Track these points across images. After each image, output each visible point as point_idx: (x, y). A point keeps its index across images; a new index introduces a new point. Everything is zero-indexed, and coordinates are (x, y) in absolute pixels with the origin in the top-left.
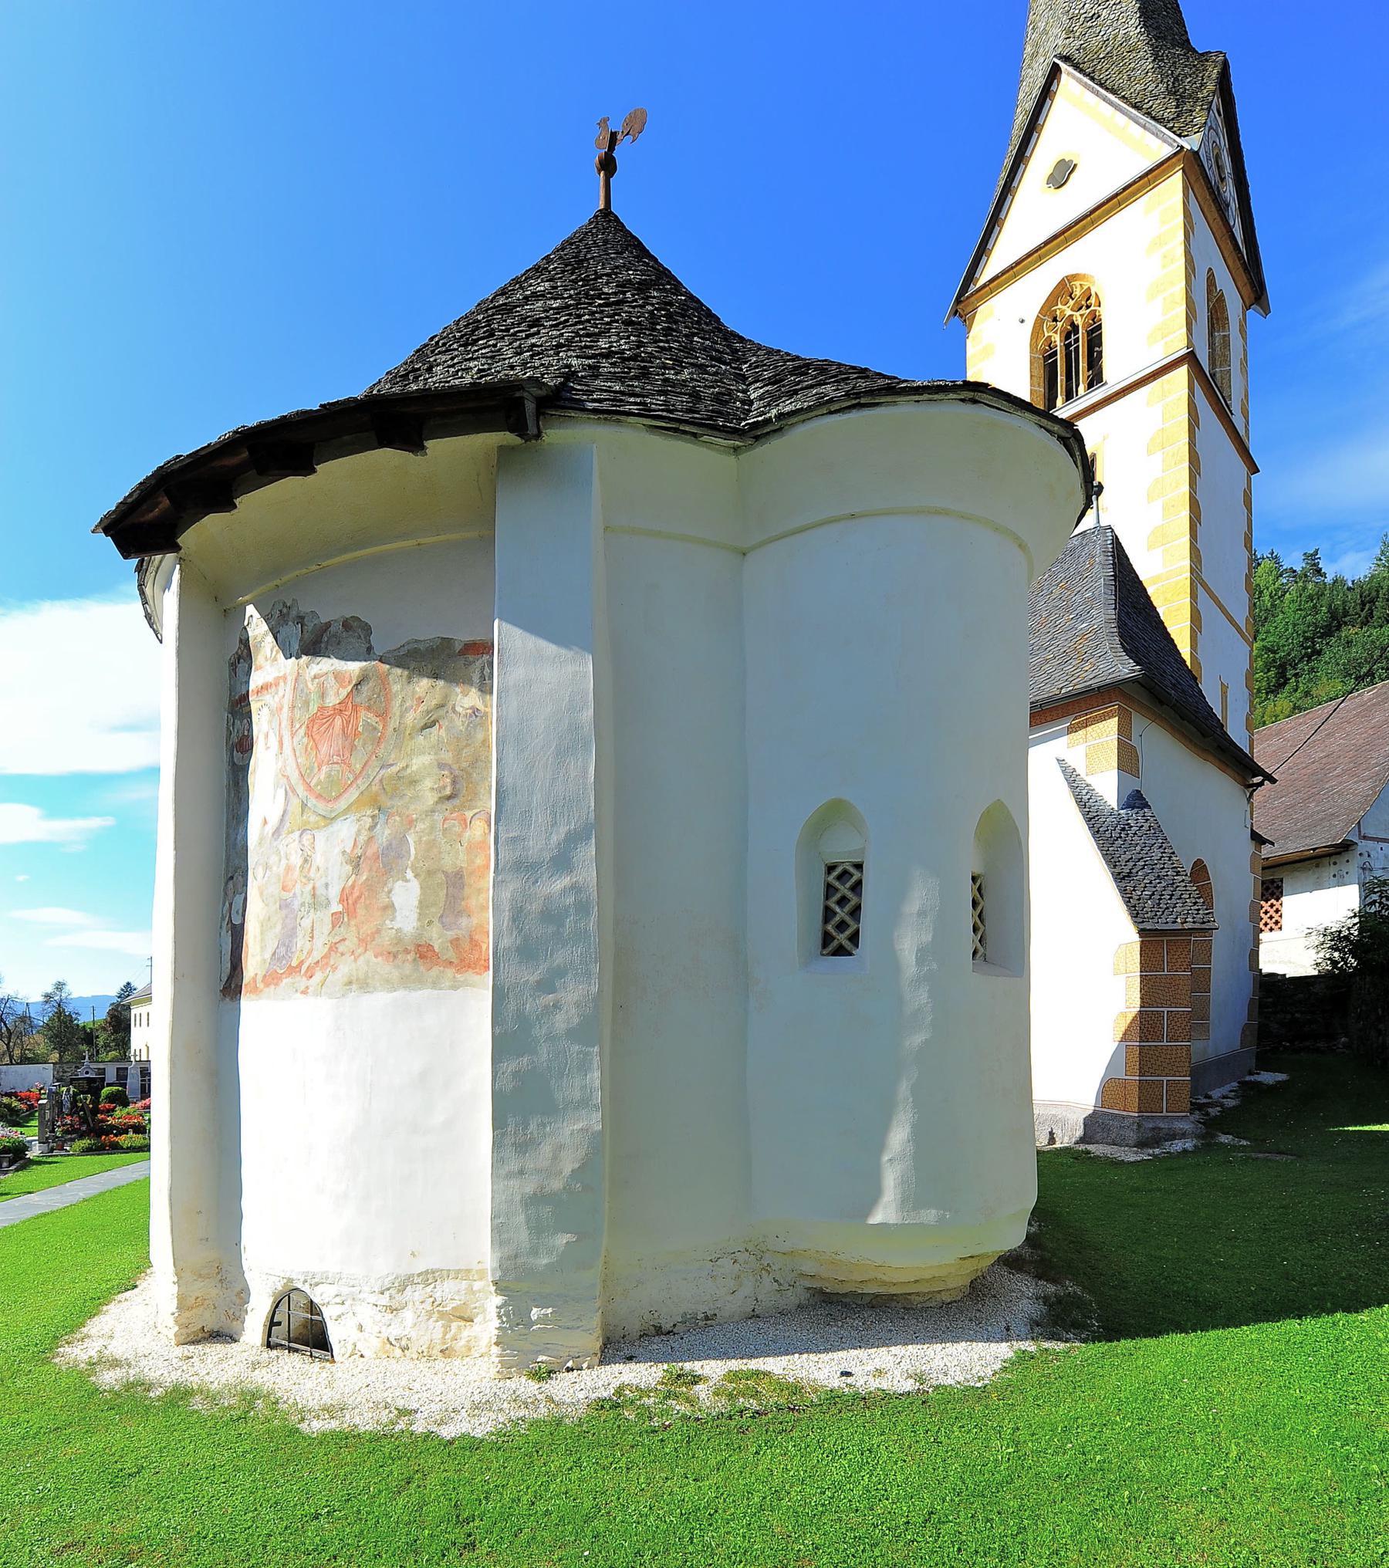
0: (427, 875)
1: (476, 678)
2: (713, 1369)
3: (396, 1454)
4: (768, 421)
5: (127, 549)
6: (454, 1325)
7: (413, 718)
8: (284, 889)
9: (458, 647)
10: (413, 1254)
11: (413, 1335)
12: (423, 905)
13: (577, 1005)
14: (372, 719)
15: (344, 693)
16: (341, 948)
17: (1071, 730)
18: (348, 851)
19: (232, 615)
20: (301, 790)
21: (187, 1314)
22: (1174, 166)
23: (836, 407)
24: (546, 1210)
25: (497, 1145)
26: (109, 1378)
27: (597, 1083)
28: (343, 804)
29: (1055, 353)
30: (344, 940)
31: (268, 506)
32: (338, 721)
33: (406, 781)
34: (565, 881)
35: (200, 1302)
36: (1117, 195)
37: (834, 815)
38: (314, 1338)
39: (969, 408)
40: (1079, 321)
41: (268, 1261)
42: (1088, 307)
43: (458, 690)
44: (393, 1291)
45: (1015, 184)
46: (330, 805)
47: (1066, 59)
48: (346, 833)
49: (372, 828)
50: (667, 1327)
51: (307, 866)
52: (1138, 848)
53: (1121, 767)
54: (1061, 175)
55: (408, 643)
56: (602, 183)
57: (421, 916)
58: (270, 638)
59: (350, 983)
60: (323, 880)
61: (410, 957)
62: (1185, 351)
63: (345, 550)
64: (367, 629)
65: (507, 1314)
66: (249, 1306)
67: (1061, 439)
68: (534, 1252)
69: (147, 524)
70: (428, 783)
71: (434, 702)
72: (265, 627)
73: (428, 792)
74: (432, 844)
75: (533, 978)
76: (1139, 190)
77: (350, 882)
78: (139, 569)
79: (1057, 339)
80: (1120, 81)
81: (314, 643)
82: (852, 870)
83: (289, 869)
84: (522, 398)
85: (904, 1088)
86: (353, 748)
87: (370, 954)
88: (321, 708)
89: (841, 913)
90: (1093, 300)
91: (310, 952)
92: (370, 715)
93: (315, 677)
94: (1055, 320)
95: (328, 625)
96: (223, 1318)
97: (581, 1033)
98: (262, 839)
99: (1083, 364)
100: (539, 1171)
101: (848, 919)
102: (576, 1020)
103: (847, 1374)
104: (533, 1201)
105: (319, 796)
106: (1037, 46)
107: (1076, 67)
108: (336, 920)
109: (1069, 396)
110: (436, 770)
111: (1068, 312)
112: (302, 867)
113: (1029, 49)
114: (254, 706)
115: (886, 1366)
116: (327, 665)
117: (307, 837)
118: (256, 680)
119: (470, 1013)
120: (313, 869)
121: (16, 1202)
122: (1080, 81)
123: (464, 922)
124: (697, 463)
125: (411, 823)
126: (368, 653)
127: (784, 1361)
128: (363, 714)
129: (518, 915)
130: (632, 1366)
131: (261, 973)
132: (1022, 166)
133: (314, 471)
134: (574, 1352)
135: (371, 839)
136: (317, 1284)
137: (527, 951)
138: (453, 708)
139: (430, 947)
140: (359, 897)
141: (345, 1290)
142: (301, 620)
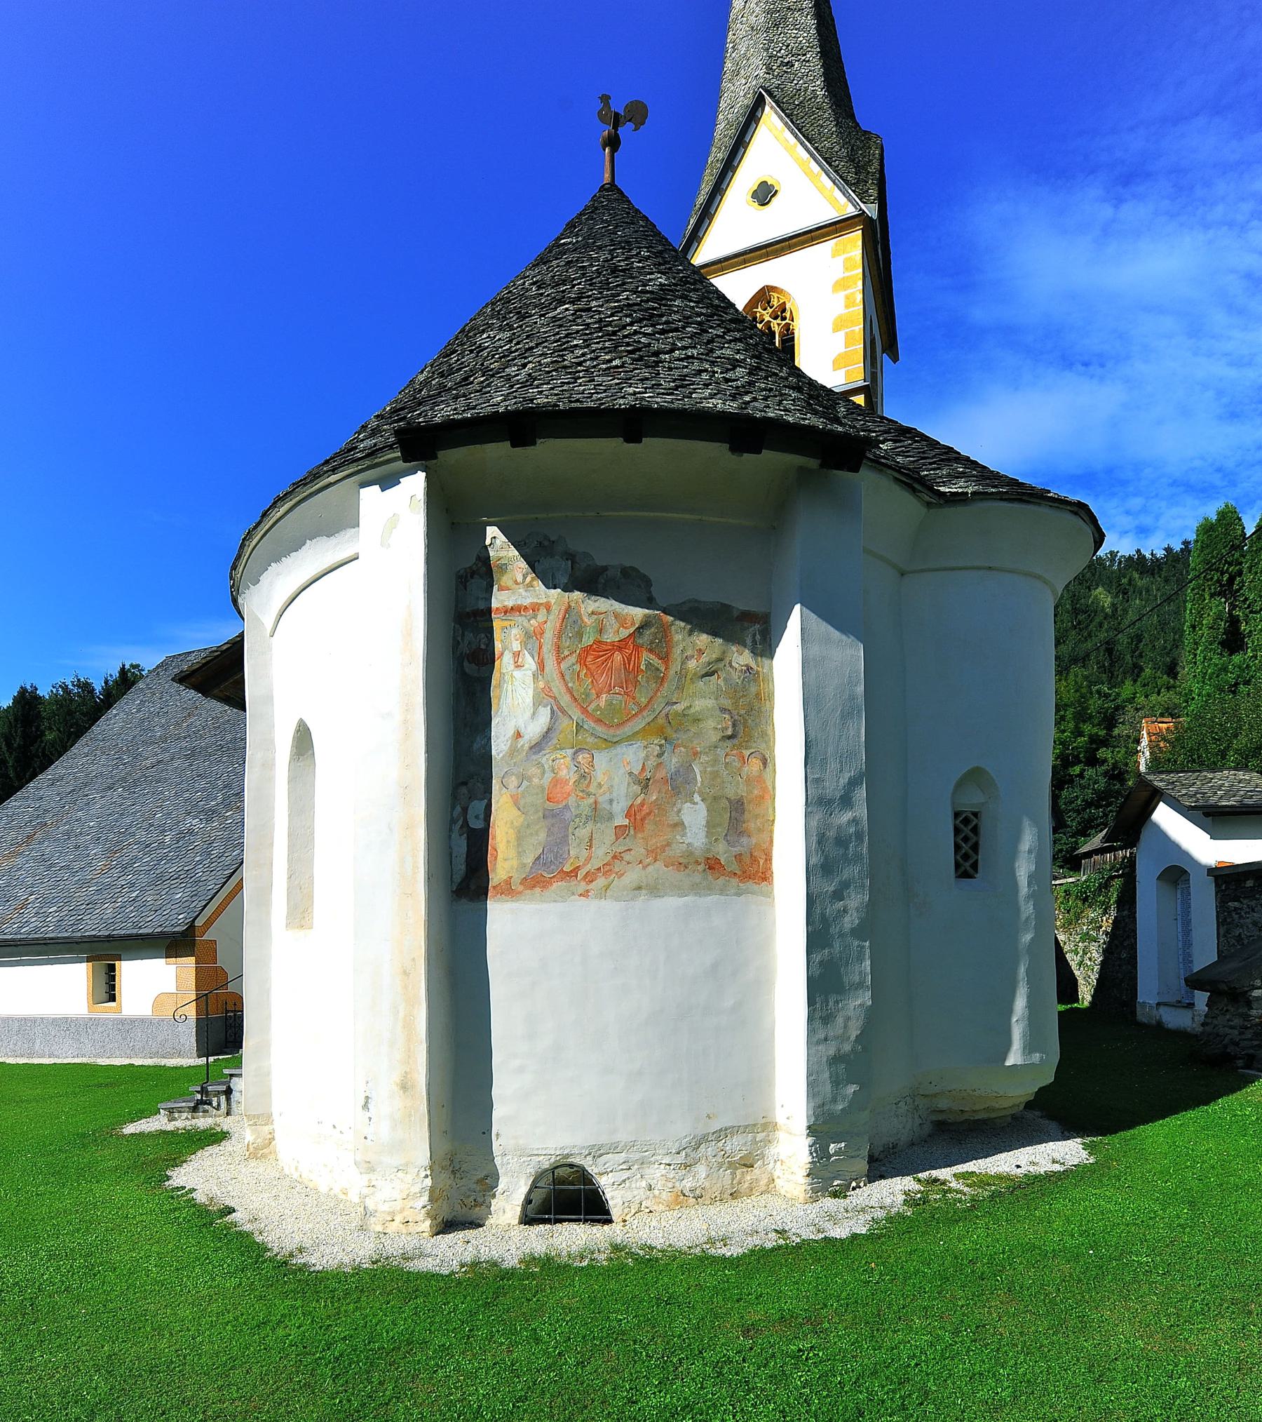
0: (713, 801)
1: (749, 642)
6: (738, 1172)
9: (736, 614)
10: (708, 1116)
11: (707, 1184)
12: (710, 825)
13: (857, 909)
14: (656, 661)
15: (624, 633)
16: (627, 857)
25: (810, 1019)
33: (688, 720)
37: (975, 776)
40: (776, 329)
46: (612, 731)
48: (633, 756)
49: (660, 755)
54: (764, 194)
55: (690, 601)
56: (607, 158)
59: (639, 888)
60: (607, 797)
61: (701, 868)
65: (816, 1151)
70: (711, 723)
71: (714, 656)
73: (712, 728)
74: (715, 775)
75: (832, 889)
77: (639, 801)
87: (659, 864)
91: (589, 859)
92: (652, 656)
93: (593, 613)
95: (605, 569)
96: (458, 1207)
98: (513, 751)
100: (836, 1038)
101: (971, 852)
104: (835, 1060)
107: (777, 102)
108: (620, 831)
110: (718, 712)
111: (767, 318)
113: (728, 65)
120: (594, 784)
123: (744, 840)
125: (695, 754)
126: (648, 602)
128: (646, 656)
136: (601, 1155)
138: (730, 663)
139: (718, 861)
140: (649, 814)
142: (571, 557)
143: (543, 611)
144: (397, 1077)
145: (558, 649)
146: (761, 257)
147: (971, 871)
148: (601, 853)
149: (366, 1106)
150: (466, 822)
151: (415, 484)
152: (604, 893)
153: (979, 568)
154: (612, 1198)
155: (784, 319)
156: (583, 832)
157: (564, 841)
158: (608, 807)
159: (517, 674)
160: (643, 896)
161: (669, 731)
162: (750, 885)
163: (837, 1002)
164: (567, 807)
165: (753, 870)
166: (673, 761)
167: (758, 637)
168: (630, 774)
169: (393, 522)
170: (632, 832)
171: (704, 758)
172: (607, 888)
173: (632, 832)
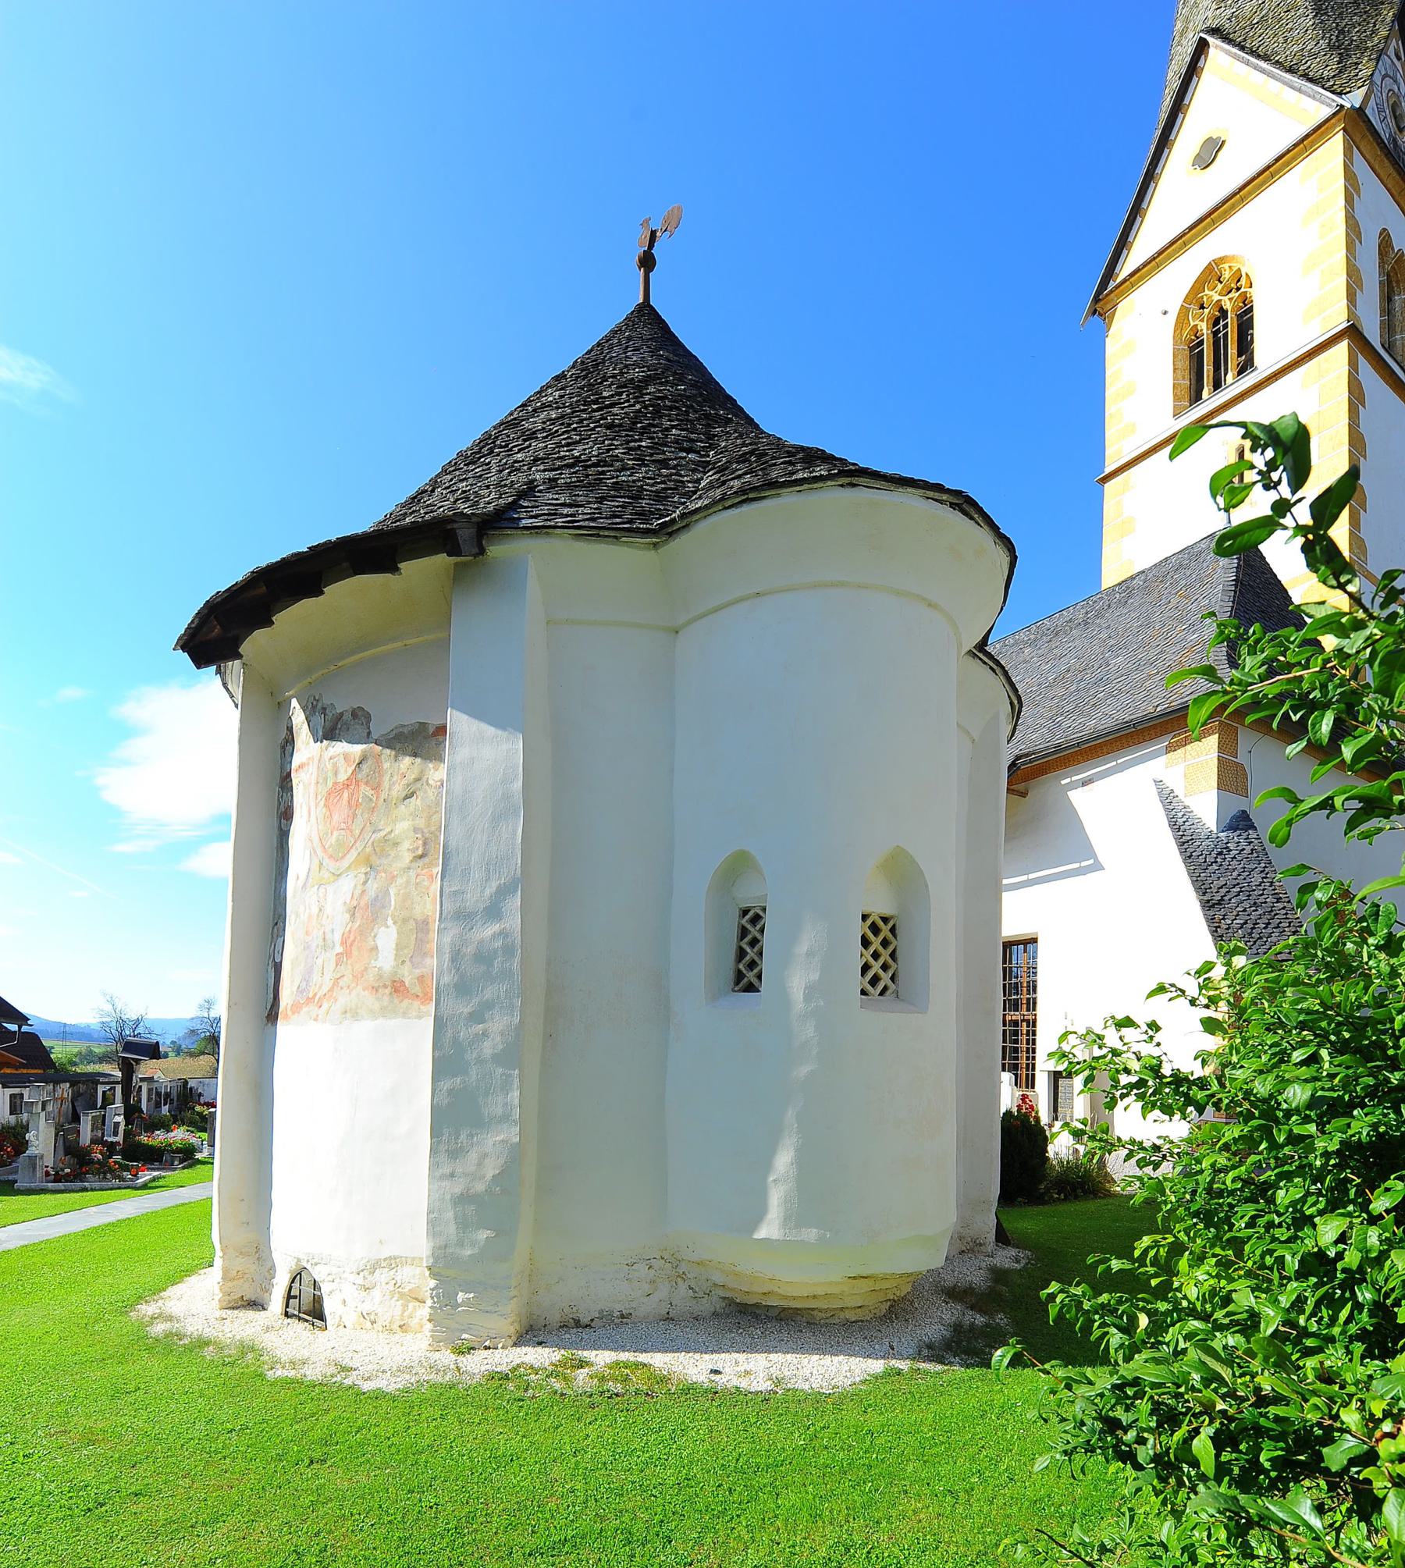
2: (602, 1358)
3: (329, 1396)
4: (673, 521)
5: (200, 661)
6: (411, 1305)
7: (398, 790)
8: (307, 933)
9: (431, 730)
12: (399, 947)
13: (502, 1033)
14: (369, 792)
15: (350, 771)
16: (341, 983)
17: (1170, 749)
19: (282, 706)
20: (320, 854)
21: (230, 1284)
22: (1334, 126)
23: (729, 503)
24: (471, 1209)
25: (433, 1151)
26: (159, 1328)
27: (516, 1101)
28: (346, 863)
29: (1201, 343)
31: (296, 620)
32: (346, 795)
33: (388, 844)
34: (496, 928)
35: (240, 1275)
36: (1269, 167)
37: (739, 866)
38: (316, 1313)
39: (849, 491)
40: (1228, 306)
41: (289, 1244)
42: (1238, 289)
43: (431, 765)
44: (366, 1273)
45: (1158, 170)
47: (1215, 31)
48: (346, 887)
49: (365, 883)
50: (585, 1320)
52: (1235, 874)
53: (1221, 786)
54: (1209, 153)
58: (306, 725)
61: (387, 991)
62: (1345, 325)
63: (353, 653)
64: (368, 717)
66: (275, 1281)
67: (952, 505)
68: (460, 1244)
69: (214, 636)
72: (302, 716)
76: (1294, 159)
78: (218, 672)
79: (1204, 327)
80: (1272, 45)
81: (330, 731)
83: (310, 917)
84: (454, 529)
85: (790, 1115)
86: (355, 816)
87: (360, 988)
88: (335, 783)
89: (751, 953)
90: (1243, 281)
94: (1202, 307)
95: (342, 714)
97: (510, 1056)
99: (1232, 350)
100: (465, 1175)
102: (501, 1047)
103: (716, 1372)
104: (462, 1199)
105: (331, 857)
106: (1187, 21)
107: (1226, 38)
109: (1217, 385)
110: (412, 834)
111: (1216, 297)
113: (1179, 26)
114: (295, 782)
115: (750, 1369)
116: (340, 747)
117: (322, 890)
118: (297, 759)
119: (413, 1040)
121: (166, 1194)
122: (1228, 53)
124: (622, 562)
126: (367, 738)
127: (669, 1357)
128: (363, 787)
129: (456, 957)
130: (539, 1349)
131: (290, 1003)
132: (1166, 151)
133: (322, 593)
134: (492, 1334)
135: (363, 892)
137: (463, 988)
141: (335, 1270)
146: (1205, 229)
153: (741, 600)
161: (373, 858)
163: (471, 1136)
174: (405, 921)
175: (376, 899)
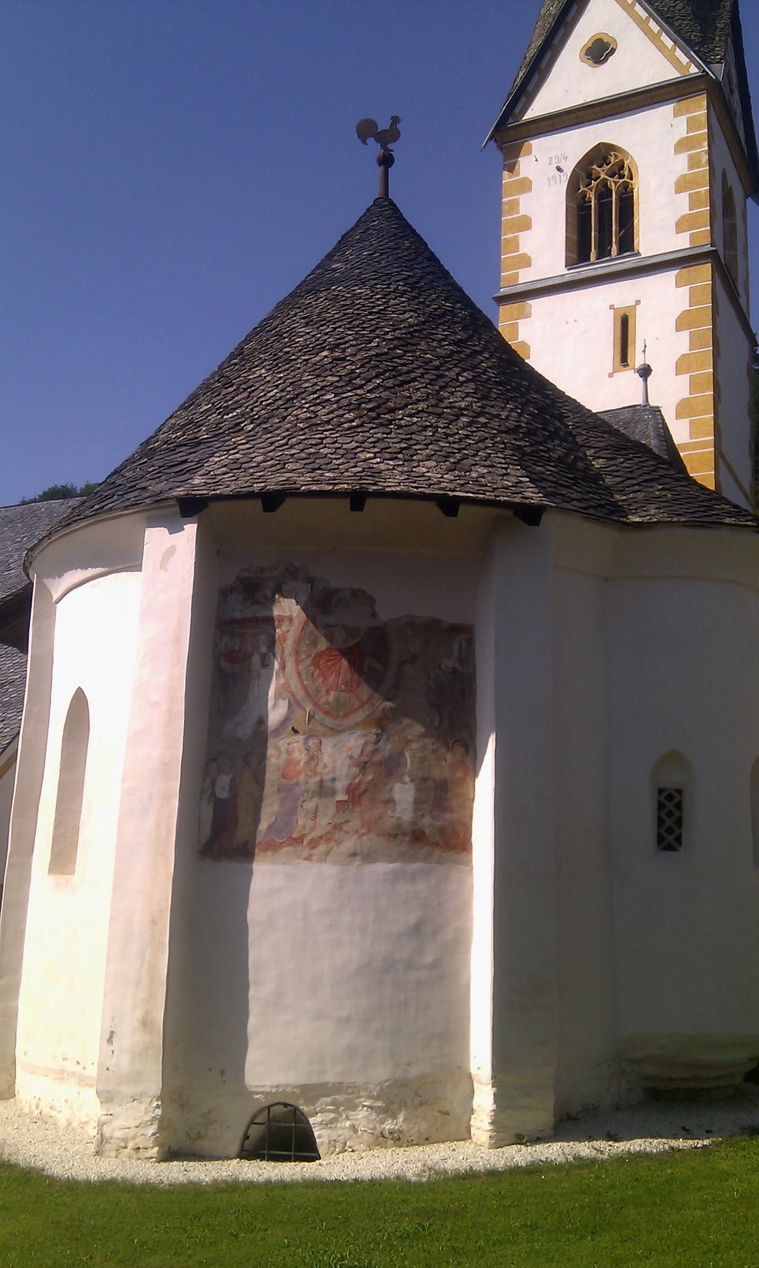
11: (404, 1127)
15: (351, 643)
16: (346, 827)
18: (355, 756)
30: (347, 822)
37: (674, 758)
51: (313, 763)
54: (600, 52)
57: (416, 810)
59: (354, 855)
60: (330, 776)
61: (407, 839)
64: (372, 601)
74: (423, 760)
77: (357, 780)
79: (592, 195)
82: (675, 793)
89: (669, 822)
91: (313, 829)
95: (338, 591)
105: (327, 713)
111: (603, 176)
112: (307, 763)
123: (447, 816)
125: (408, 742)
135: (376, 751)
139: (423, 833)
143: (287, 622)
144: (138, 1014)
145: (297, 653)
147: (674, 844)
148: (323, 823)
149: (110, 1040)
150: (213, 794)
151: (191, 529)
152: (323, 859)
154: (320, 1136)
155: (622, 177)
156: (310, 805)
157: (293, 812)
158: (330, 784)
159: (263, 671)
160: (357, 861)
162: (451, 854)
164: (297, 783)
165: (457, 842)
166: (387, 748)
167: (464, 645)
168: (351, 757)
169: (171, 552)
170: (351, 806)
171: (414, 746)
172: (328, 853)
173: (351, 806)
174: (424, 780)
175: (390, 757)
